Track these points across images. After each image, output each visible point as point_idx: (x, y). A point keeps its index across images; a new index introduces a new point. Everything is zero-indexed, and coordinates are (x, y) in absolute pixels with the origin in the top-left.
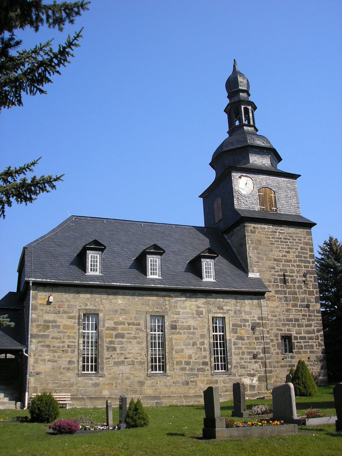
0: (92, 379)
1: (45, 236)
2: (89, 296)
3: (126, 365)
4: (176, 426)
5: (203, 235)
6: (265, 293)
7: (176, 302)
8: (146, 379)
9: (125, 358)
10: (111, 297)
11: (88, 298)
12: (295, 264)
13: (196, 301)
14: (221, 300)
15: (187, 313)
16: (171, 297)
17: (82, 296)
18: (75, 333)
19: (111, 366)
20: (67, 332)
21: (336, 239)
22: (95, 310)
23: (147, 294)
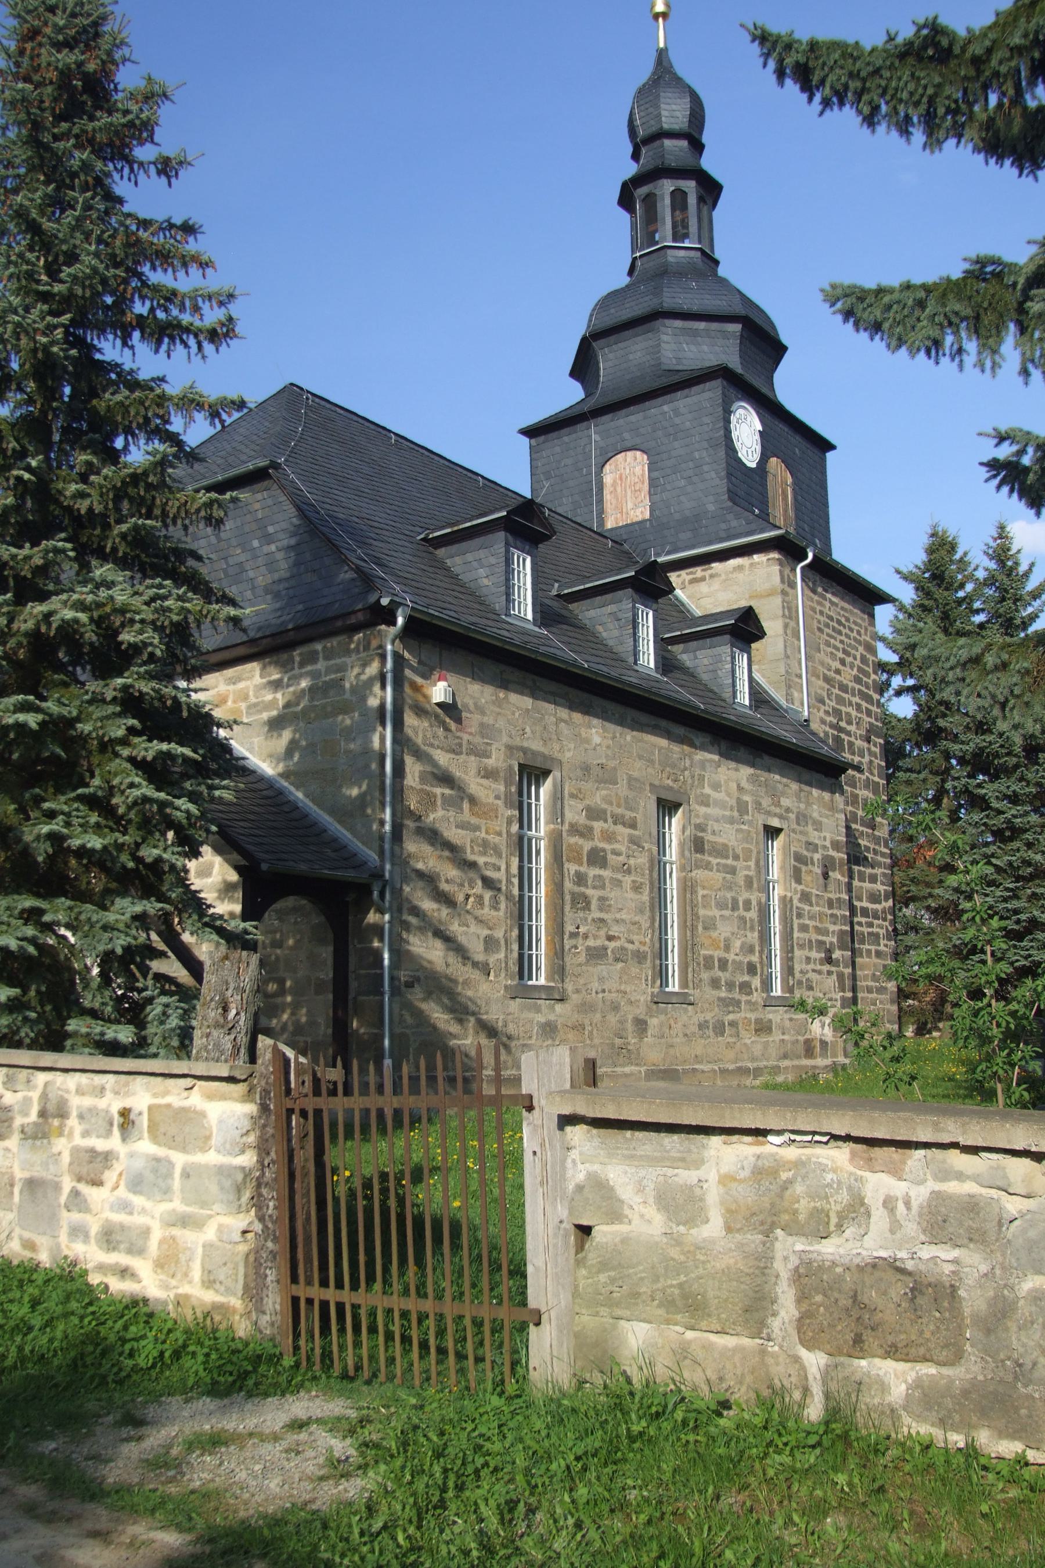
0: (538, 1010)
1: (600, 501)
2: (527, 702)
3: (611, 961)
4: (826, 876)
5: (632, 524)
6: (844, 771)
7: (703, 764)
8: (650, 1013)
9: (610, 938)
10: (577, 717)
11: (528, 710)
12: (724, 976)
13: (737, 770)
14: (777, 777)
15: (723, 805)
16: (692, 745)
17: (514, 697)
18: (499, 834)
19: (580, 965)
20: (477, 828)
21: (858, 330)
22: (544, 755)
23: (648, 725)
